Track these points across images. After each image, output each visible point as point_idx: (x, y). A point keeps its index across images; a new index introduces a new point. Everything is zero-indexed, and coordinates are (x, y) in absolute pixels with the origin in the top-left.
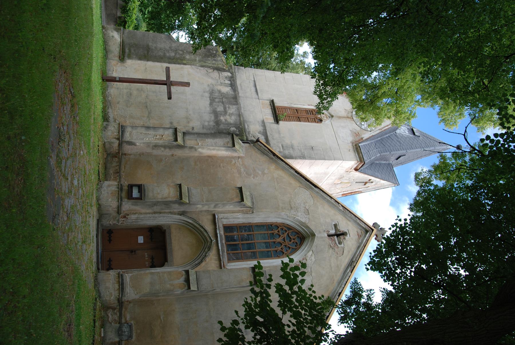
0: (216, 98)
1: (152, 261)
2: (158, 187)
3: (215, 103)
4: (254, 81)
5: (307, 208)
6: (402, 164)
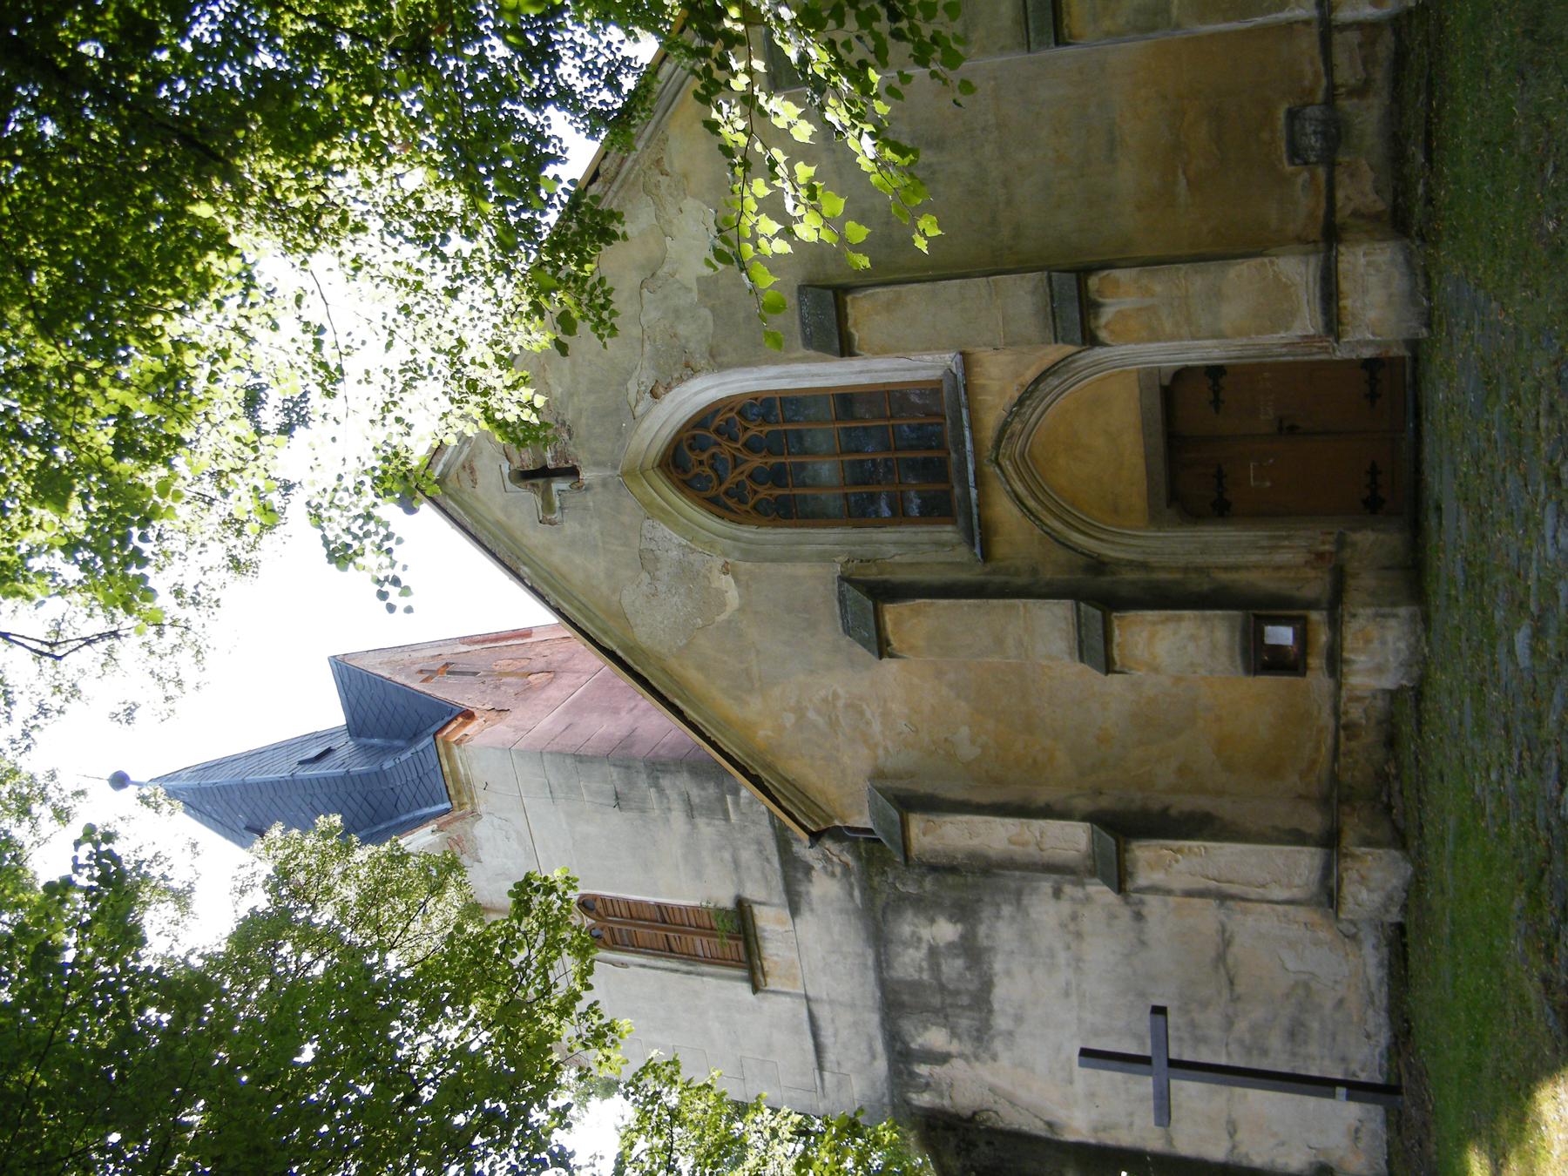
0: (970, 1007)
1: (1216, 394)
2: (1192, 664)
3: (972, 987)
4: (821, 1068)
5: (645, 576)
6: (317, 737)
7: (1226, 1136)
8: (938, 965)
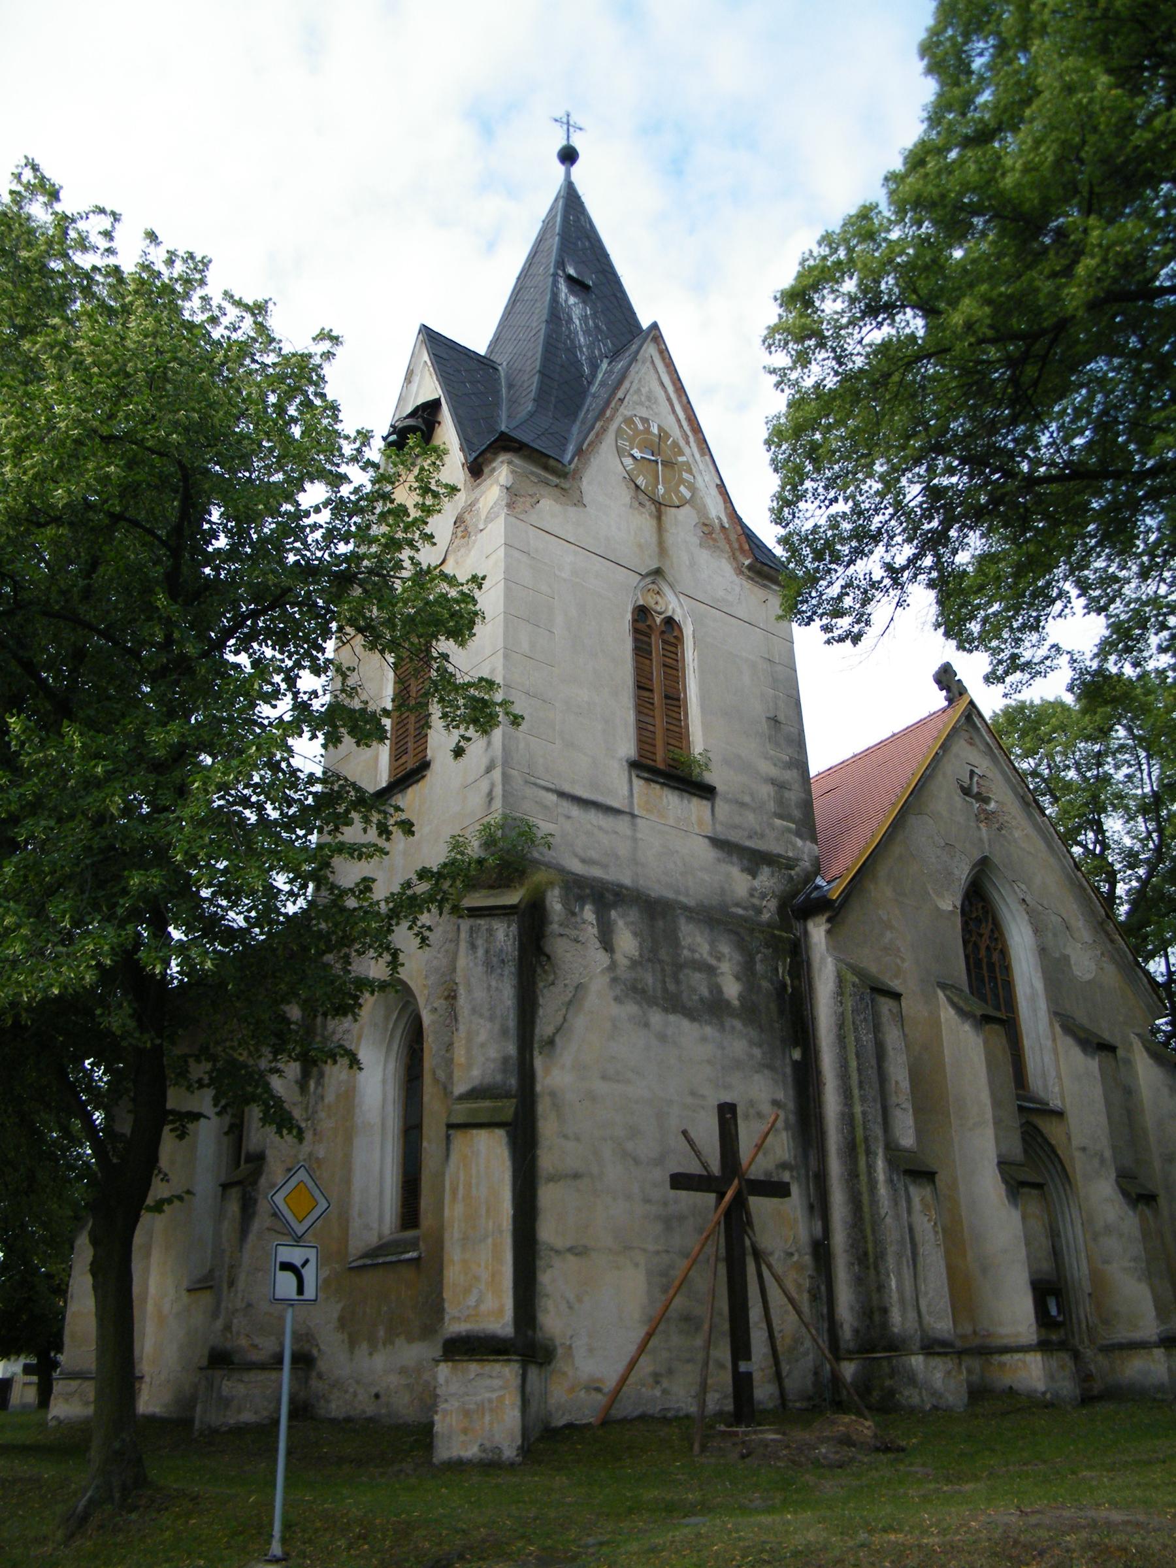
4: (562, 795)
7: (568, 1244)
8: (700, 970)
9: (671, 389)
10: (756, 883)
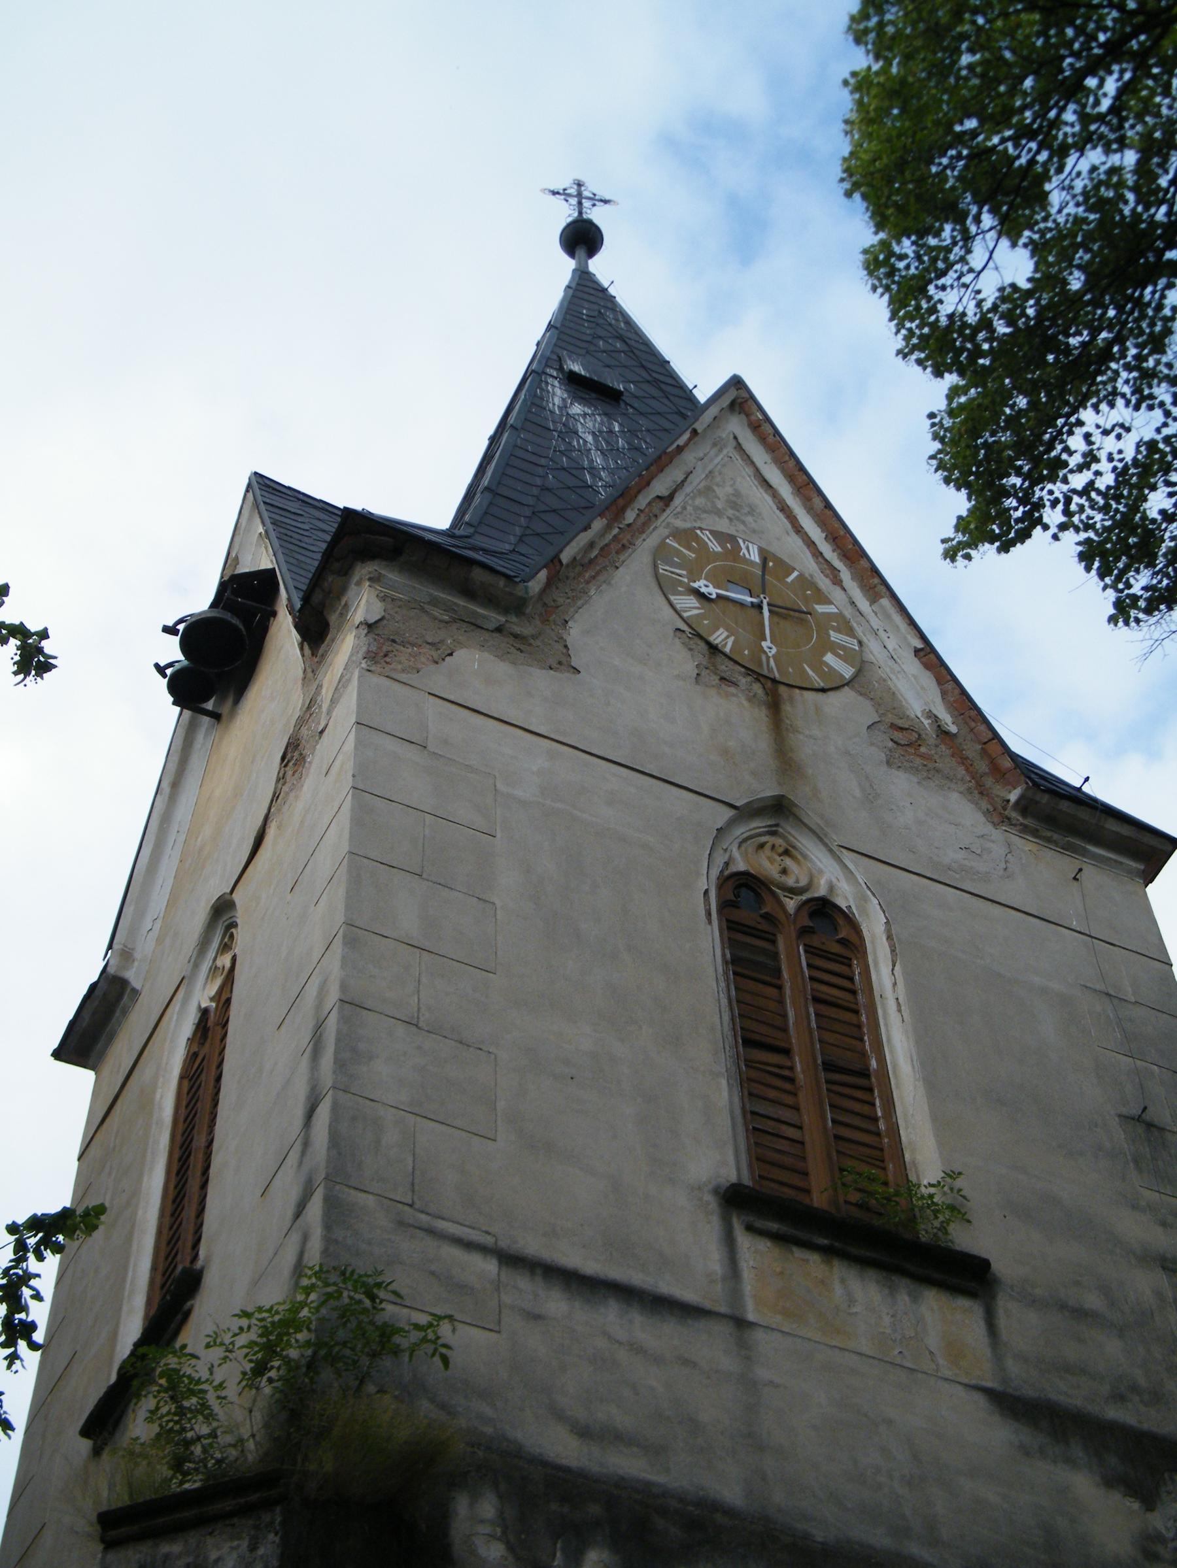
9: (785, 490)
10: (1157, 1521)
